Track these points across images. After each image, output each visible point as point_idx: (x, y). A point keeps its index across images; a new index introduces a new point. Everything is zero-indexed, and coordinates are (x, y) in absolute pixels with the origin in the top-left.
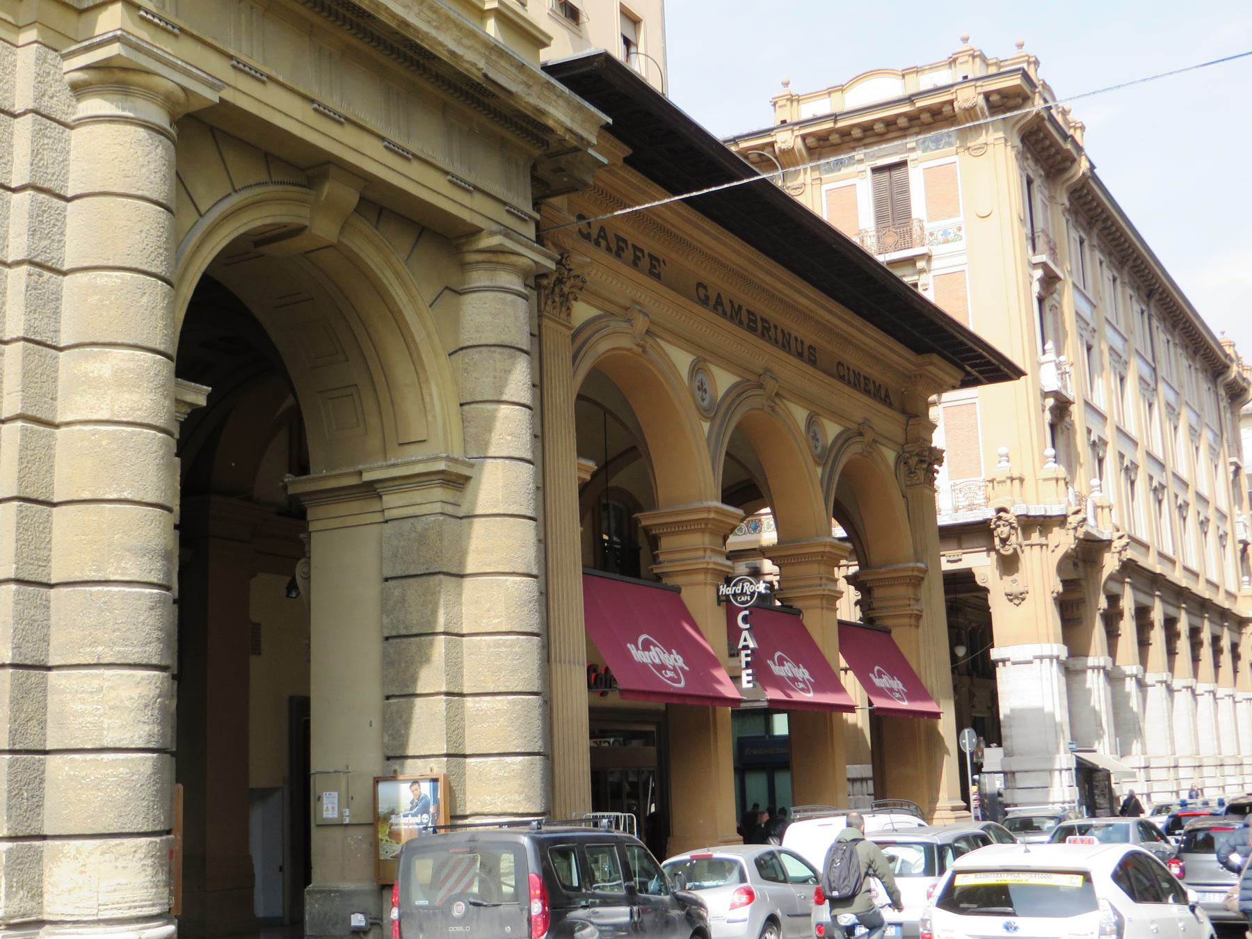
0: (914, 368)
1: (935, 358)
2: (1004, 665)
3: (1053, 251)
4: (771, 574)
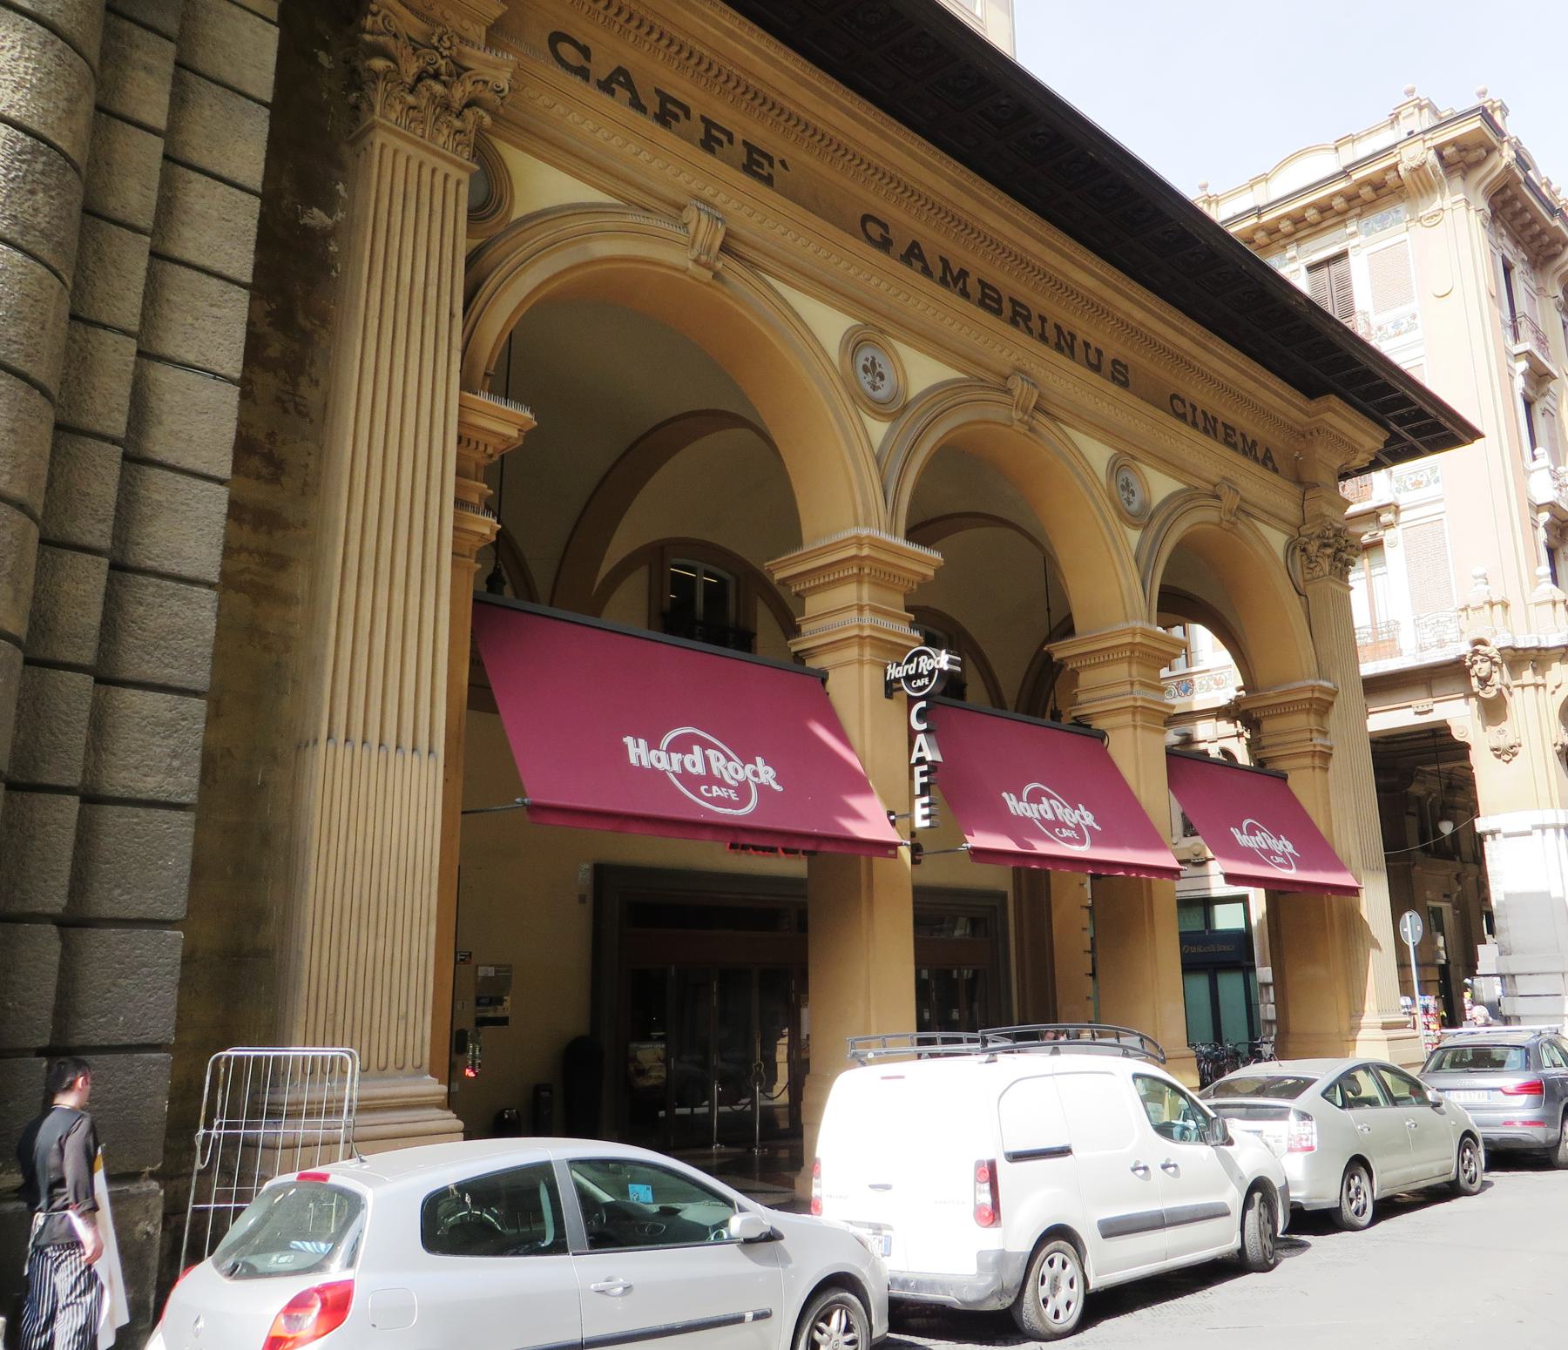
0: (1306, 418)
1: (1334, 401)
2: (1494, 839)
3: (1542, 341)
4: (1205, 741)
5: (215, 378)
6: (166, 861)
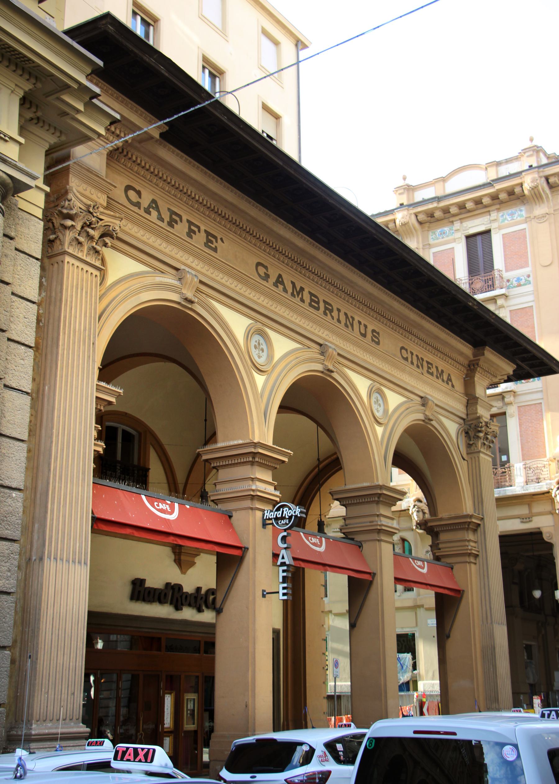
5: (22, 394)
6: (6, 620)
